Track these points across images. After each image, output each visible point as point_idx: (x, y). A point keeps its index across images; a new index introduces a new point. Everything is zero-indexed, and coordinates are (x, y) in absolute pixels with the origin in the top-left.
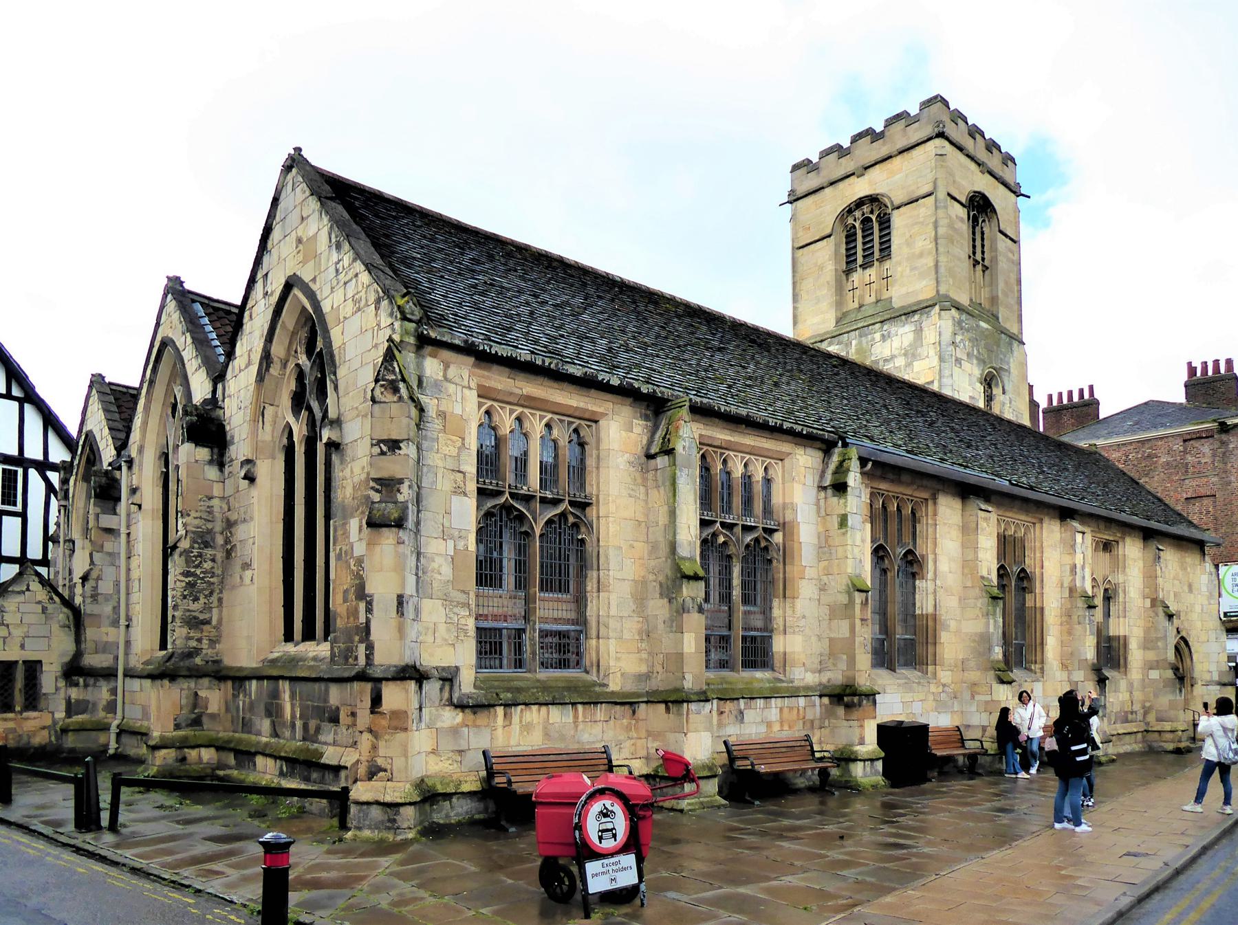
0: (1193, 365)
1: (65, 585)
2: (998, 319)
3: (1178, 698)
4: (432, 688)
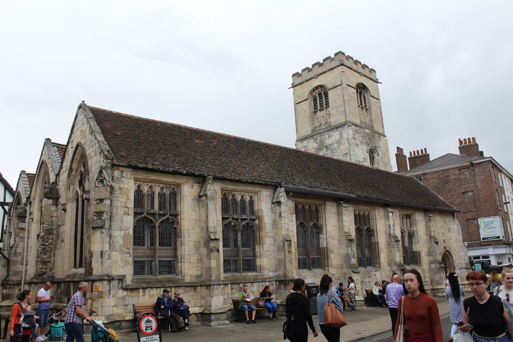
0: (461, 140)
1: (7, 249)
2: (373, 128)
3: (443, 275)
4: (115, 283)
